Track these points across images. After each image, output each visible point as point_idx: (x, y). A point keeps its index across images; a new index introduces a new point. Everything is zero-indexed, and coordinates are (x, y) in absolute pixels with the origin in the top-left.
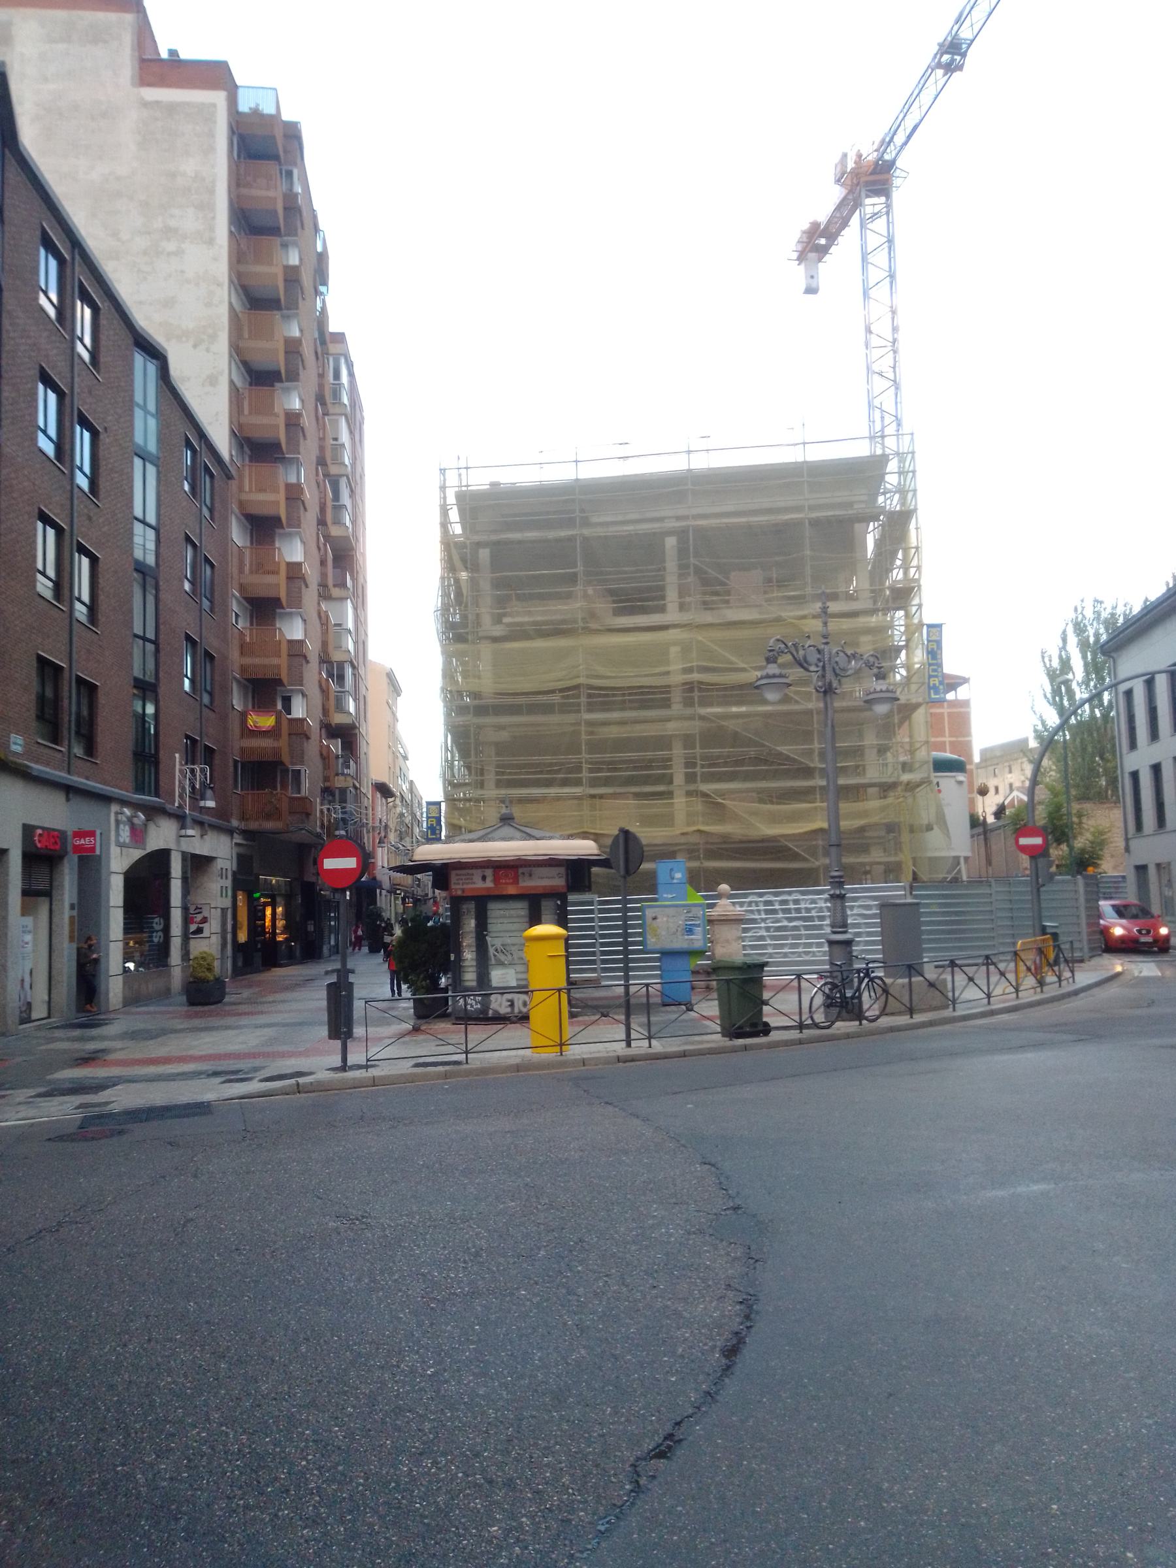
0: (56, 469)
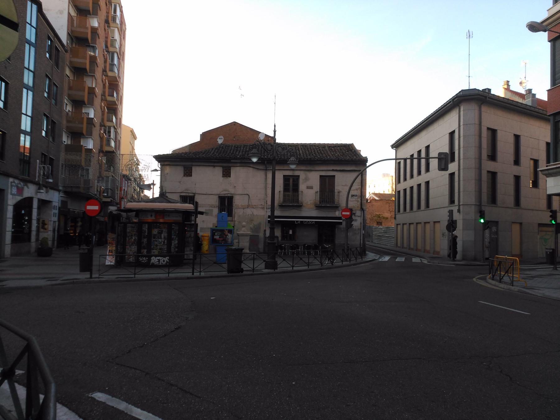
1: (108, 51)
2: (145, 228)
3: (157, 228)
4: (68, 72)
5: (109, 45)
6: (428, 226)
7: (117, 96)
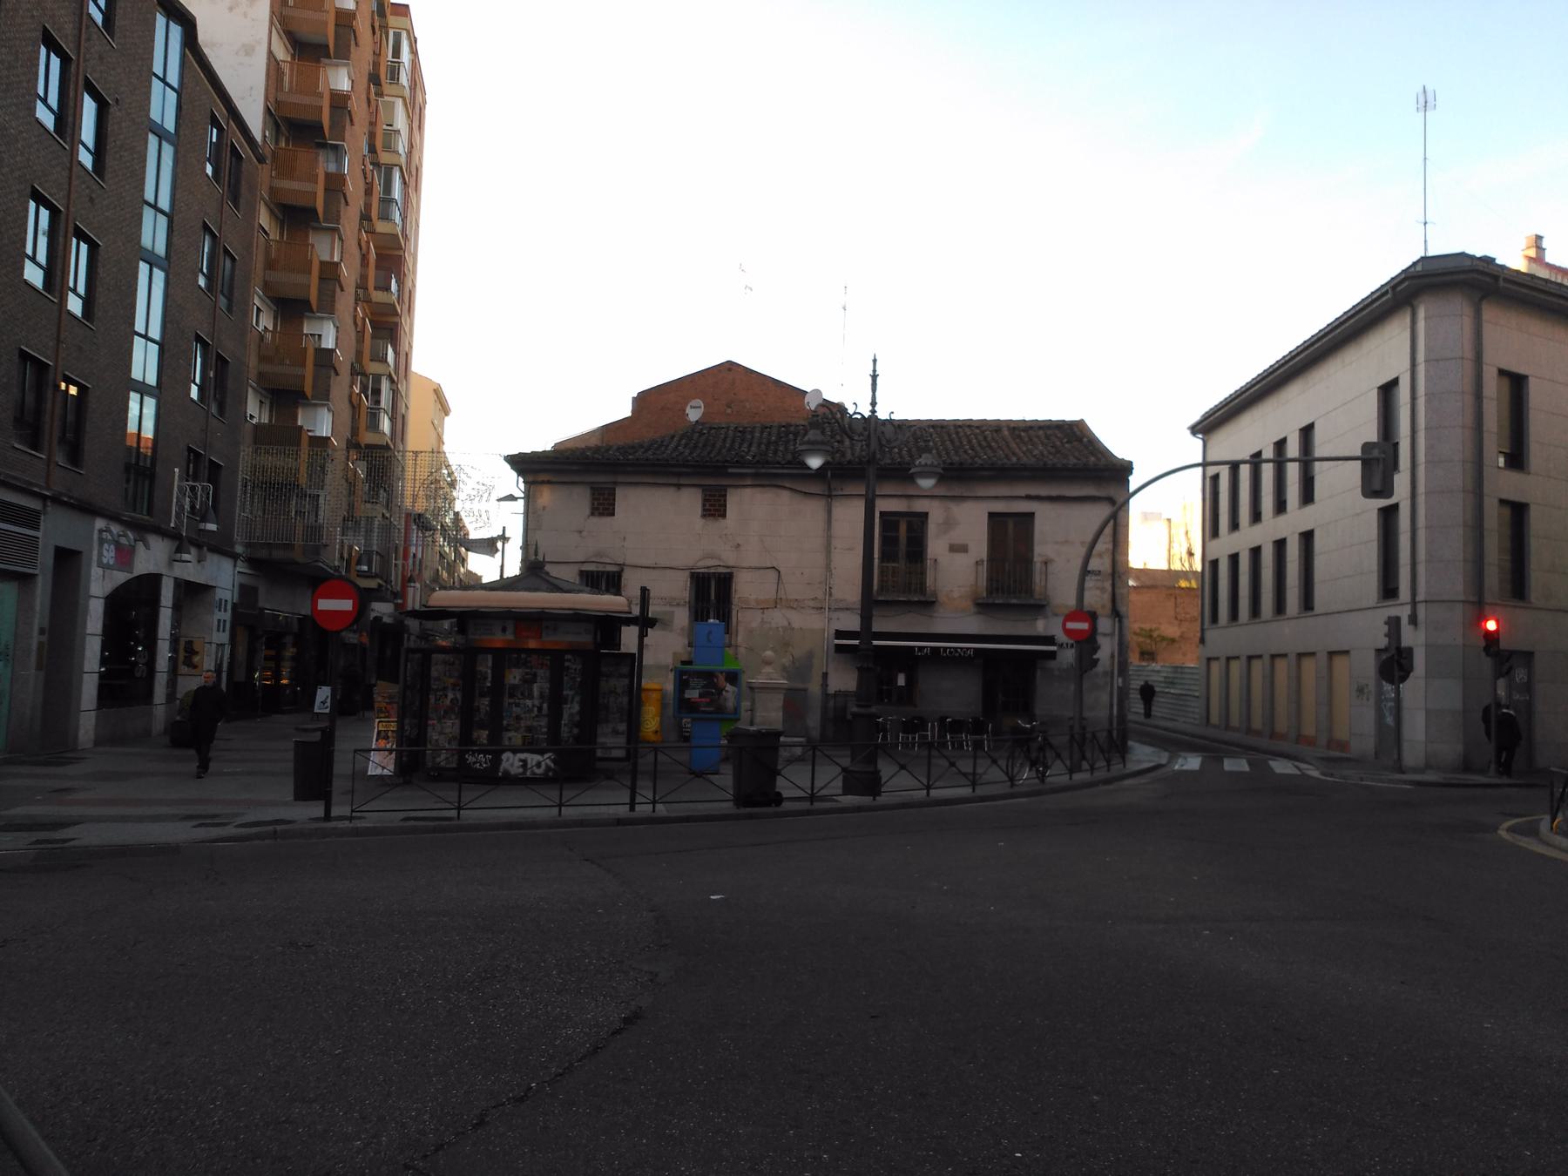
0: (48, 301)
1: (376, 164)
2: (486, 666)
3: (519, 668)
4: (264, 219)
5: (379, 144)
6: (1281, 665)
7: (399, 291)
